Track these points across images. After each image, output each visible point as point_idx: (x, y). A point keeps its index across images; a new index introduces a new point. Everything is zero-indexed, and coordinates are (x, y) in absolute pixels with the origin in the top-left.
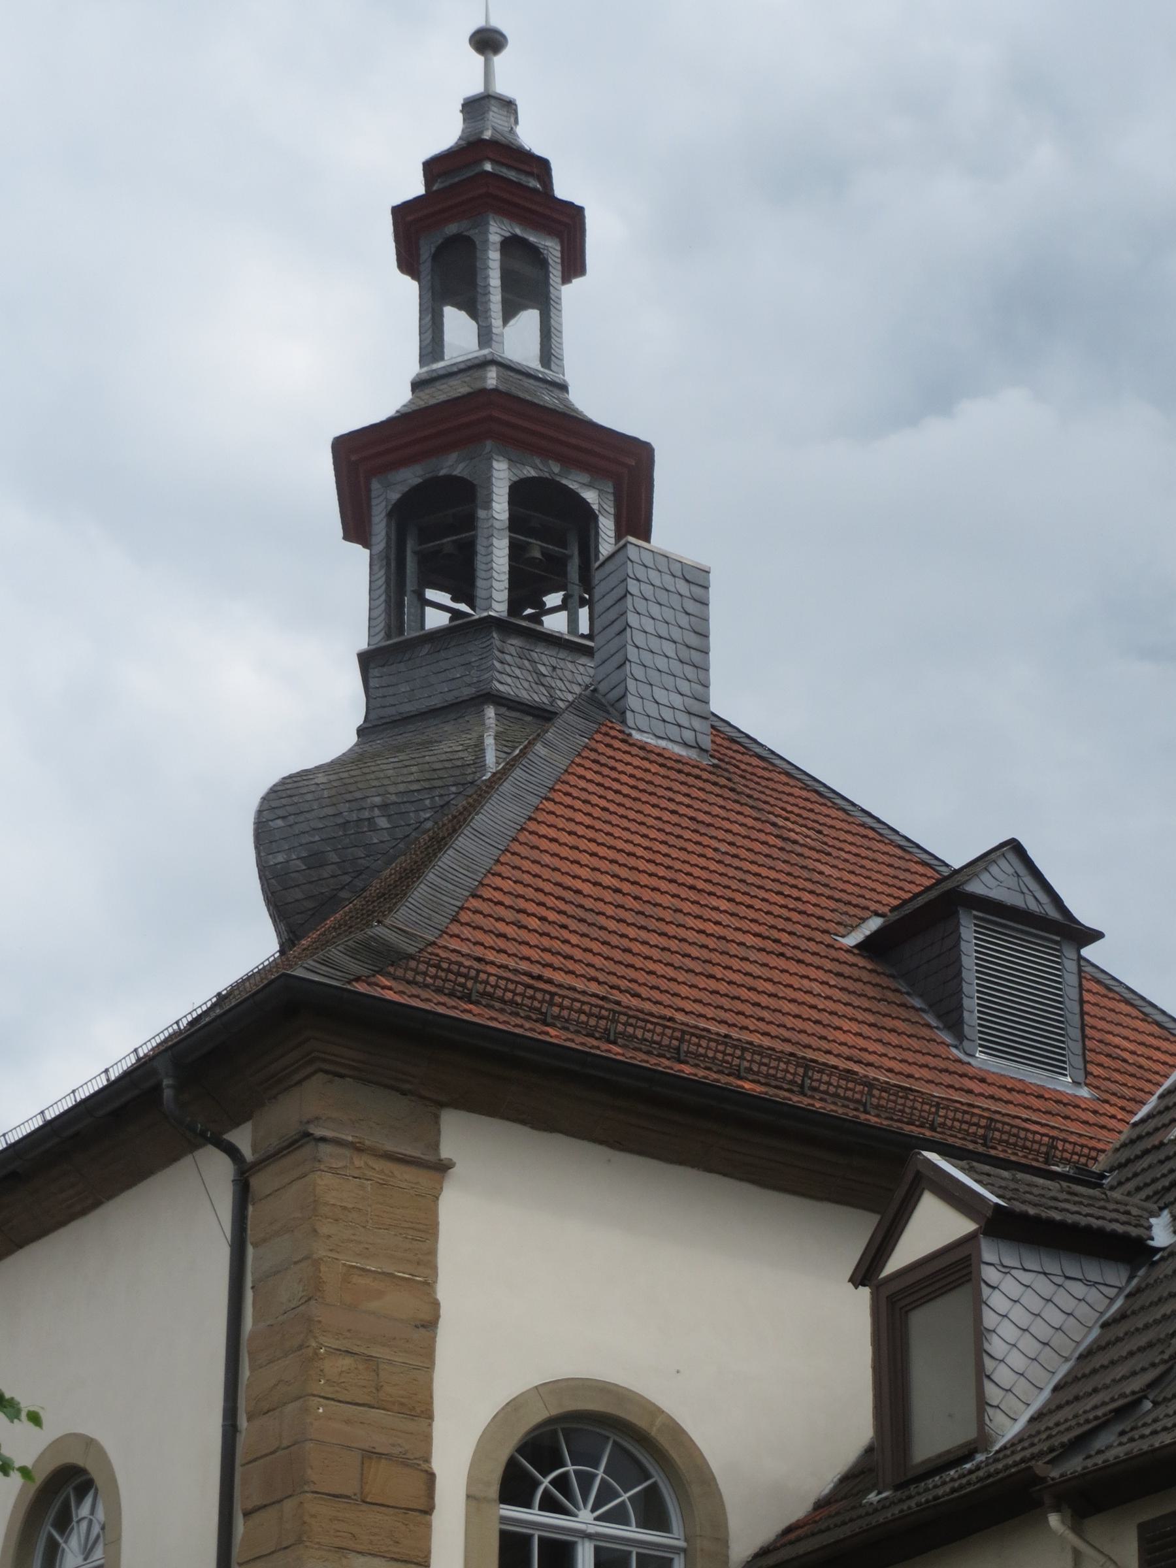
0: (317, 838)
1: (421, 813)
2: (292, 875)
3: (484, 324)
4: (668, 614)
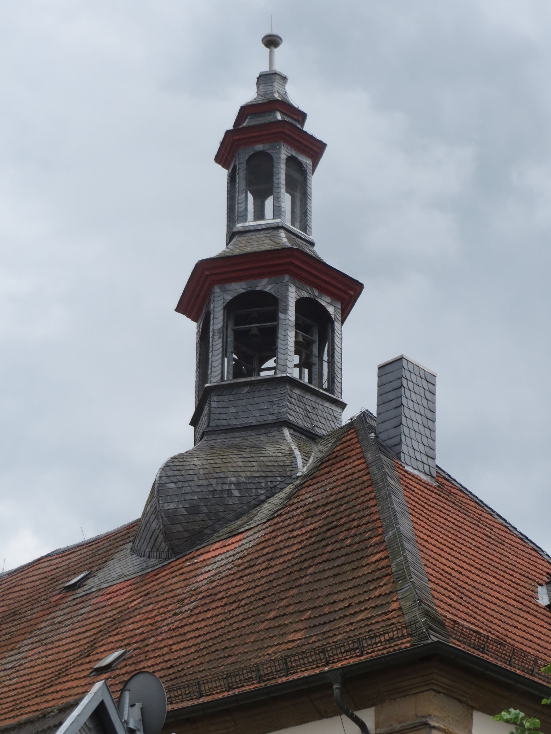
0: (196, 497)
1: (259, 491)
2: (178, 517)
3: (277, 205)
4: (419, 399)
